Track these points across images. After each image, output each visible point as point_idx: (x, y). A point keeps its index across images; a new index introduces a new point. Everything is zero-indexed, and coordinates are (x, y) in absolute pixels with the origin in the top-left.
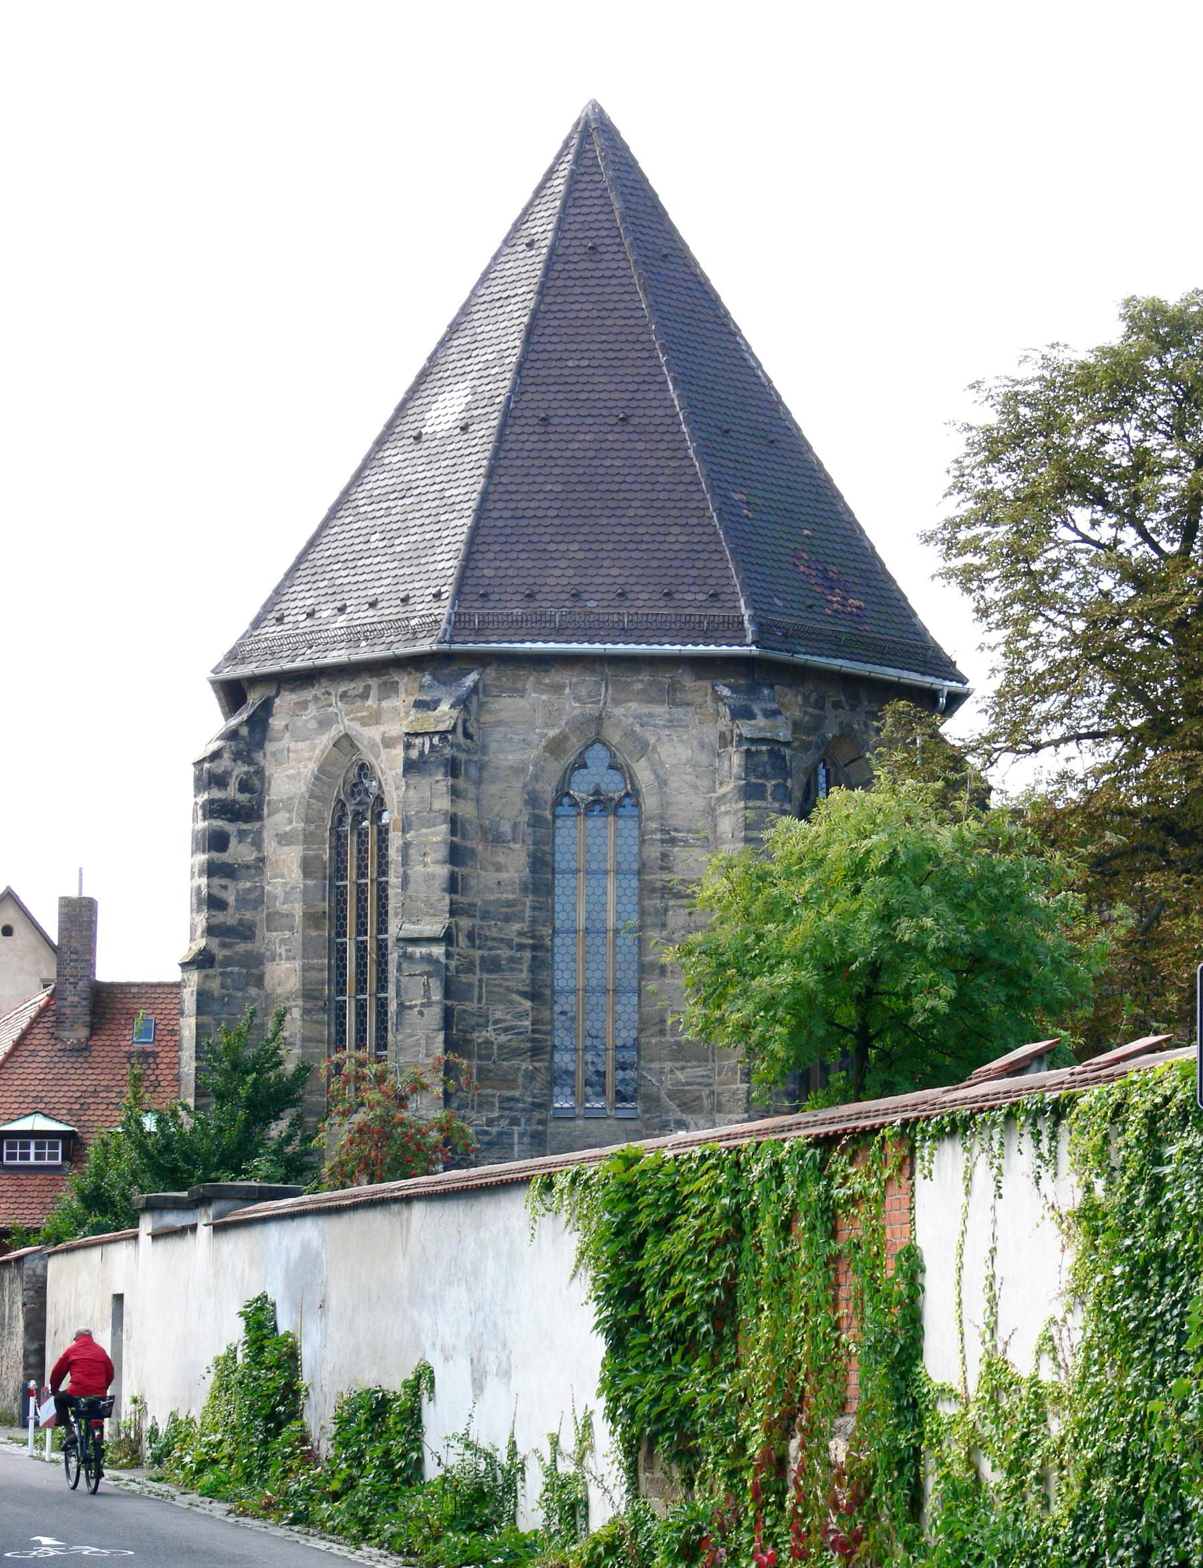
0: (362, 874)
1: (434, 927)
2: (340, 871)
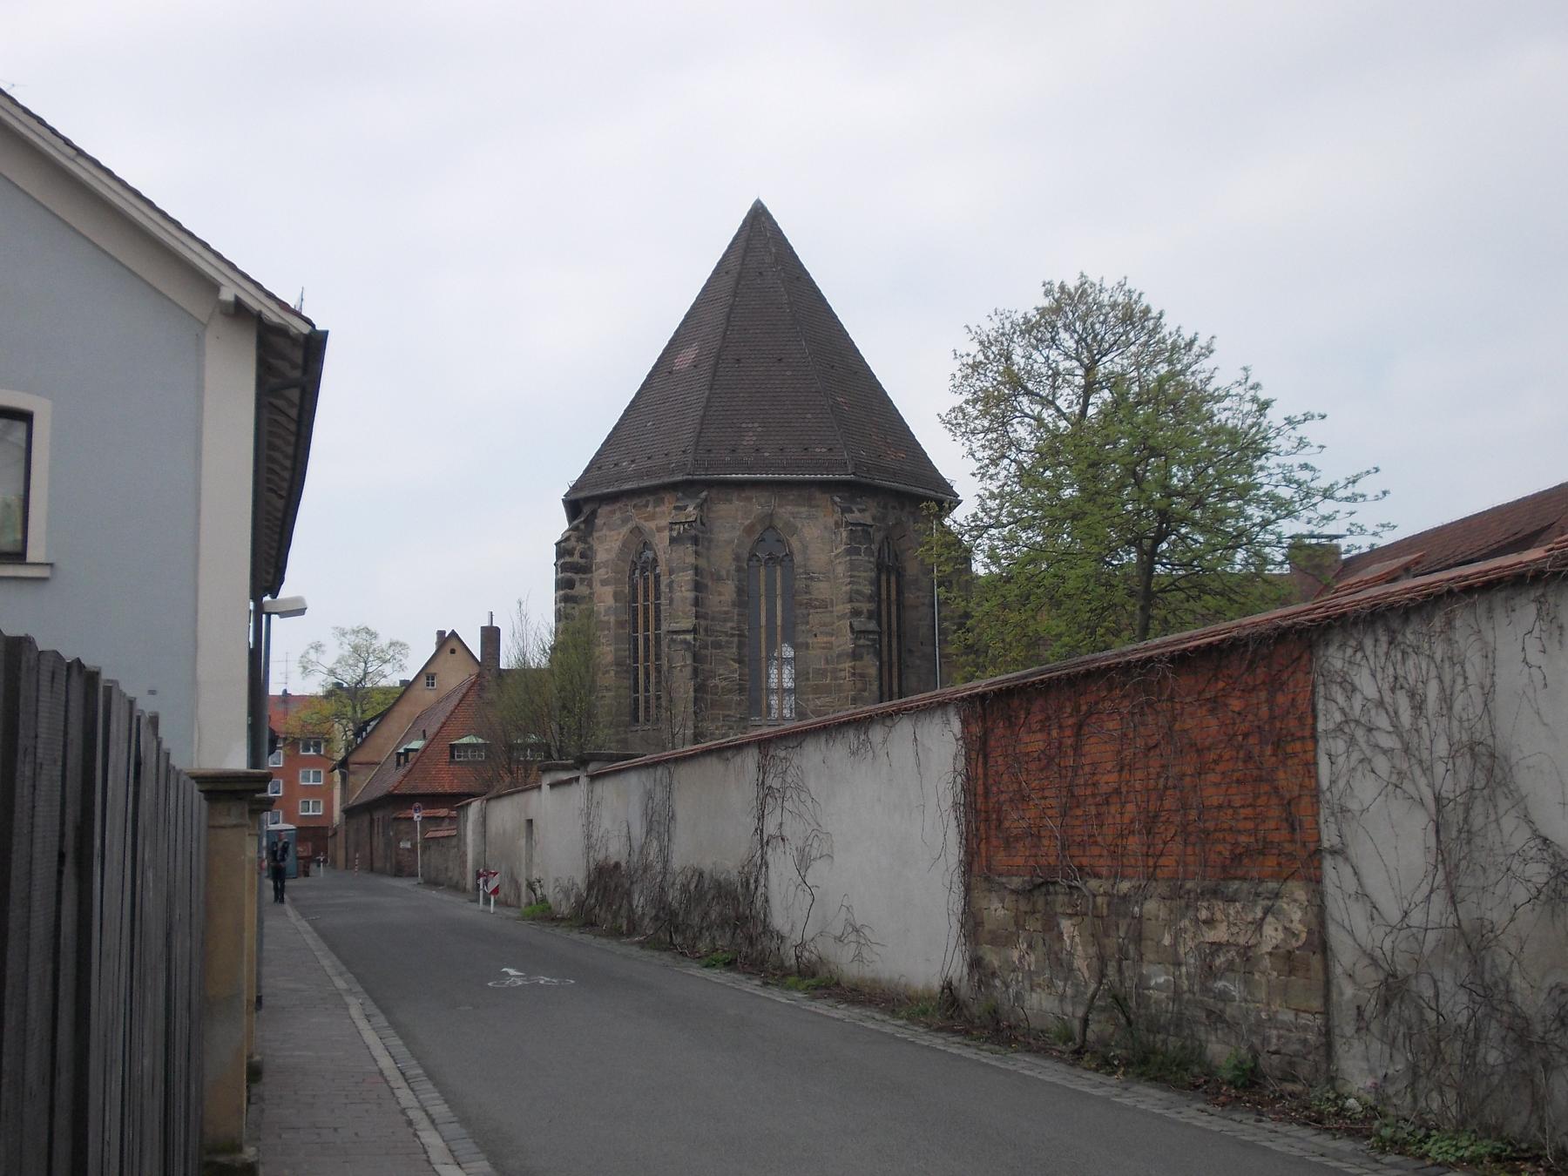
0: (646, 599)
1: (687, 624)
2: (635, 600)
